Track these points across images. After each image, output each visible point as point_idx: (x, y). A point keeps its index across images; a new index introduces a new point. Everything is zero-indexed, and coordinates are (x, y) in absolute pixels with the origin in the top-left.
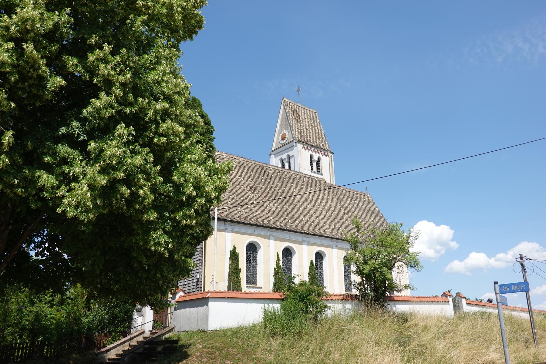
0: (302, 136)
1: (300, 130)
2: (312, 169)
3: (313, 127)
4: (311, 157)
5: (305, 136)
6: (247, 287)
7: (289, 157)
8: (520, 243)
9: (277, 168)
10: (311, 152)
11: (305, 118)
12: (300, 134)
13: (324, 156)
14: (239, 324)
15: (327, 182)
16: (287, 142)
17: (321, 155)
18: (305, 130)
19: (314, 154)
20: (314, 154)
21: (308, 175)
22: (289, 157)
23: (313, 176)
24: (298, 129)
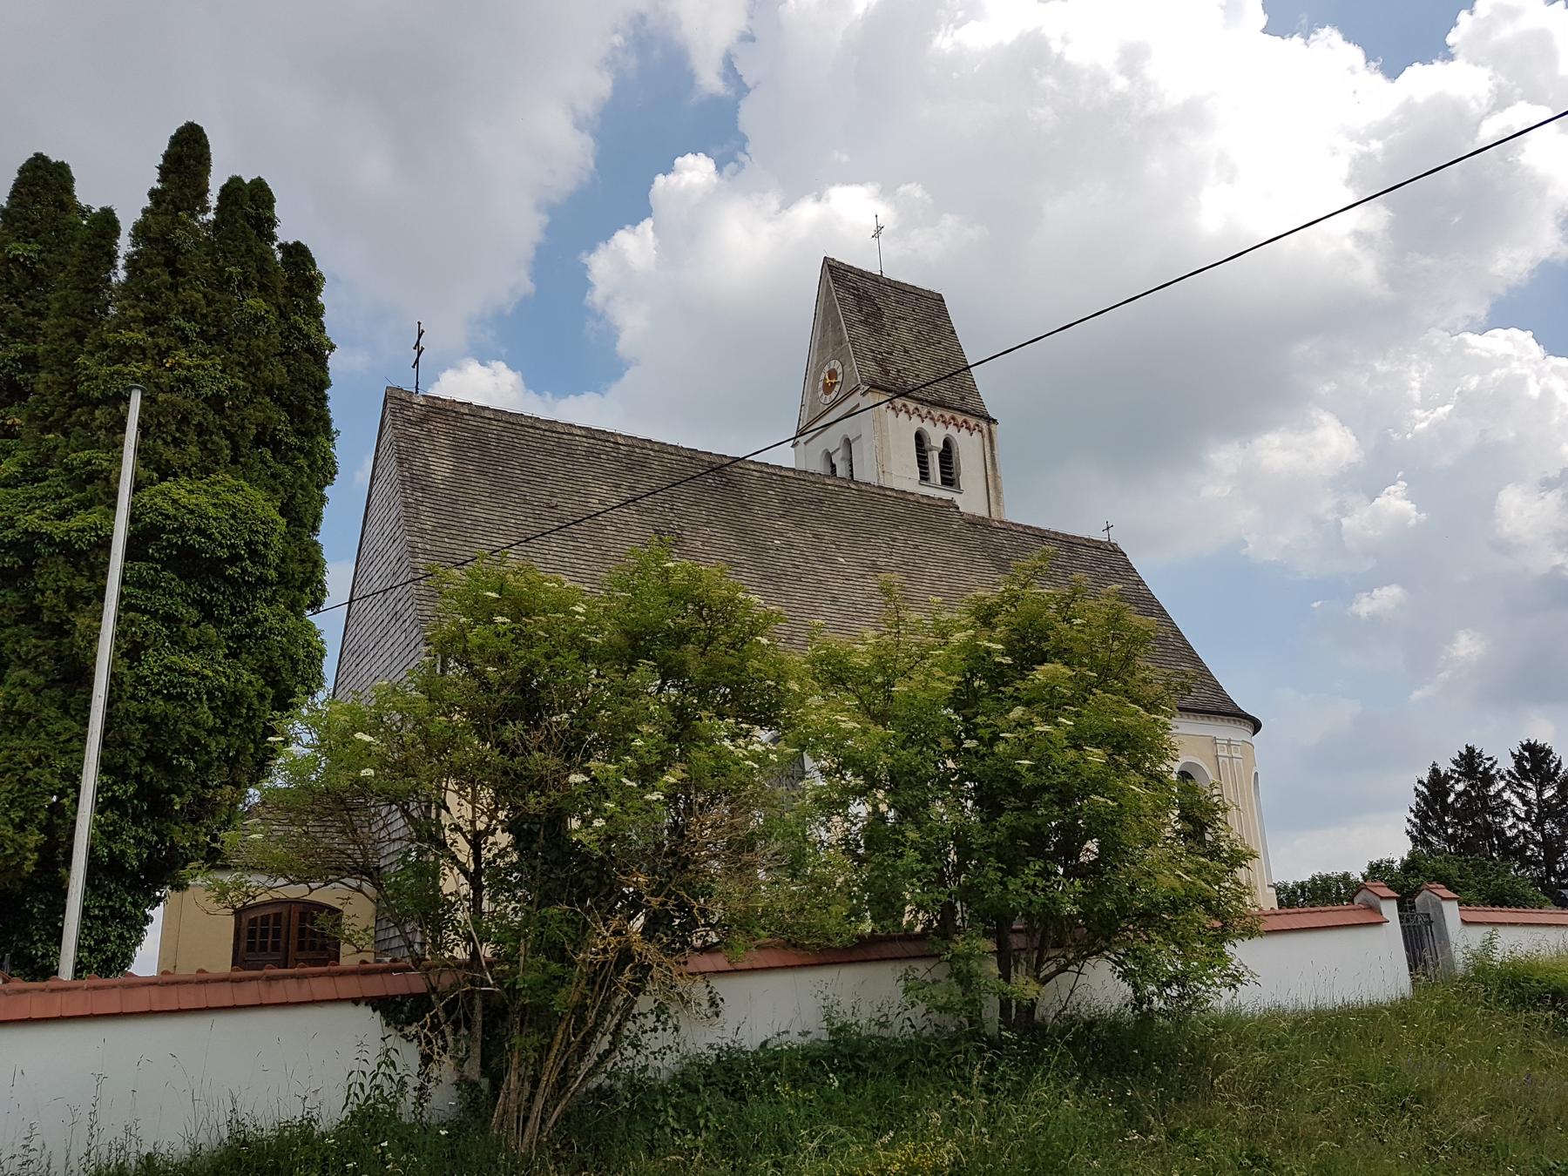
0: (887, 373)
1: (880, 353)
2: (924, 476)
3: (929, 345)
4: (920, 438)
5: (899, 371)
6: (1465, 922)
7: (848, 443)
8: (567, 396)
9: (777, 471)
10: (916, 423)
11: (900, 317)
12: (880, 365)
13: (963, 430)
14: (1293, 994)
15: (961, 510)
16: (839, 397)
17: (952, 430)
18: (898, 355)
19: (927, 426)
20: (927, 426)
21: (893, 490)
22: (848, 443)
23: (913, 494)
24: (873, 351)
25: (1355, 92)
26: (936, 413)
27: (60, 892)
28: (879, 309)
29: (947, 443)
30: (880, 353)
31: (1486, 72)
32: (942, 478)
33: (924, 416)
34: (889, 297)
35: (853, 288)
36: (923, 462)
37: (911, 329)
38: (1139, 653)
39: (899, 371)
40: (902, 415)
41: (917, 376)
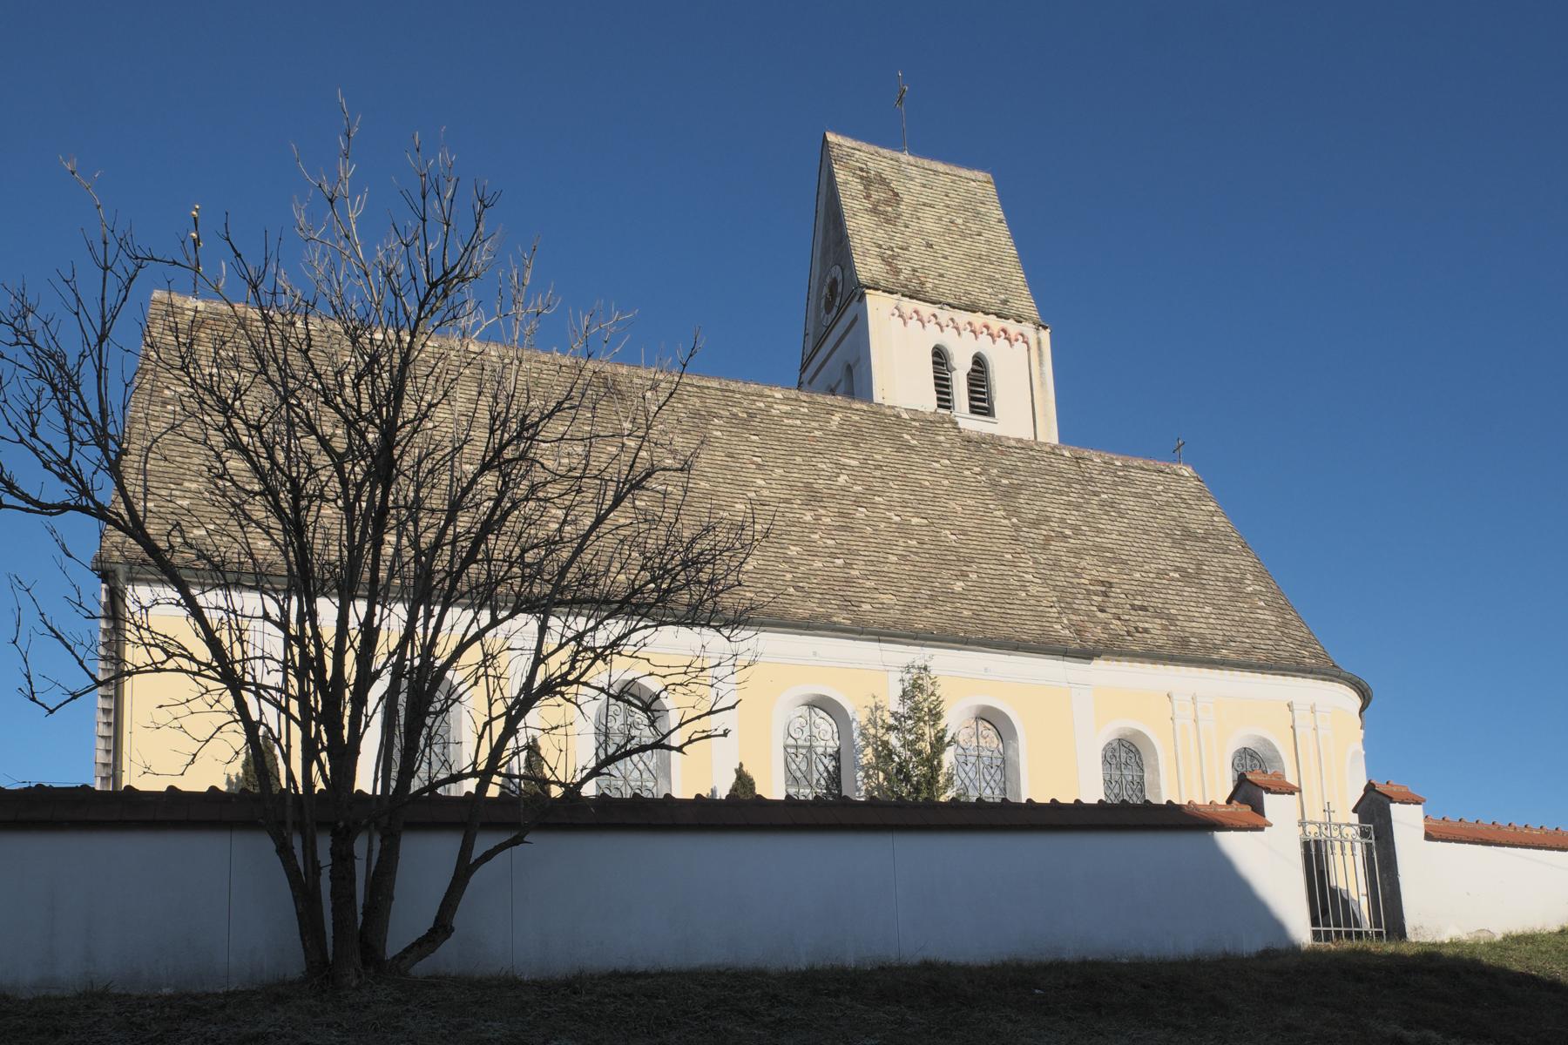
0: (897, 272)
1: (891, 249)
4: (940, 357)
12: (889, 264)
19: (949, 340)
24: (880, 247)
25: (1468, 894)
26: (963, 317)
27: (1379, 872)
28: (897, 195)
29: (979, 362)
30: (891, 249)
31: (318, 600)
32: (971, 406)
33: (944, 324)
34: (912, 179)
35: (861, 170)
36: (943, 385)
37: (940, 219)
38: (160, 336)
39: (914, 270)
40: (914, 324)
41: (941, 275)
